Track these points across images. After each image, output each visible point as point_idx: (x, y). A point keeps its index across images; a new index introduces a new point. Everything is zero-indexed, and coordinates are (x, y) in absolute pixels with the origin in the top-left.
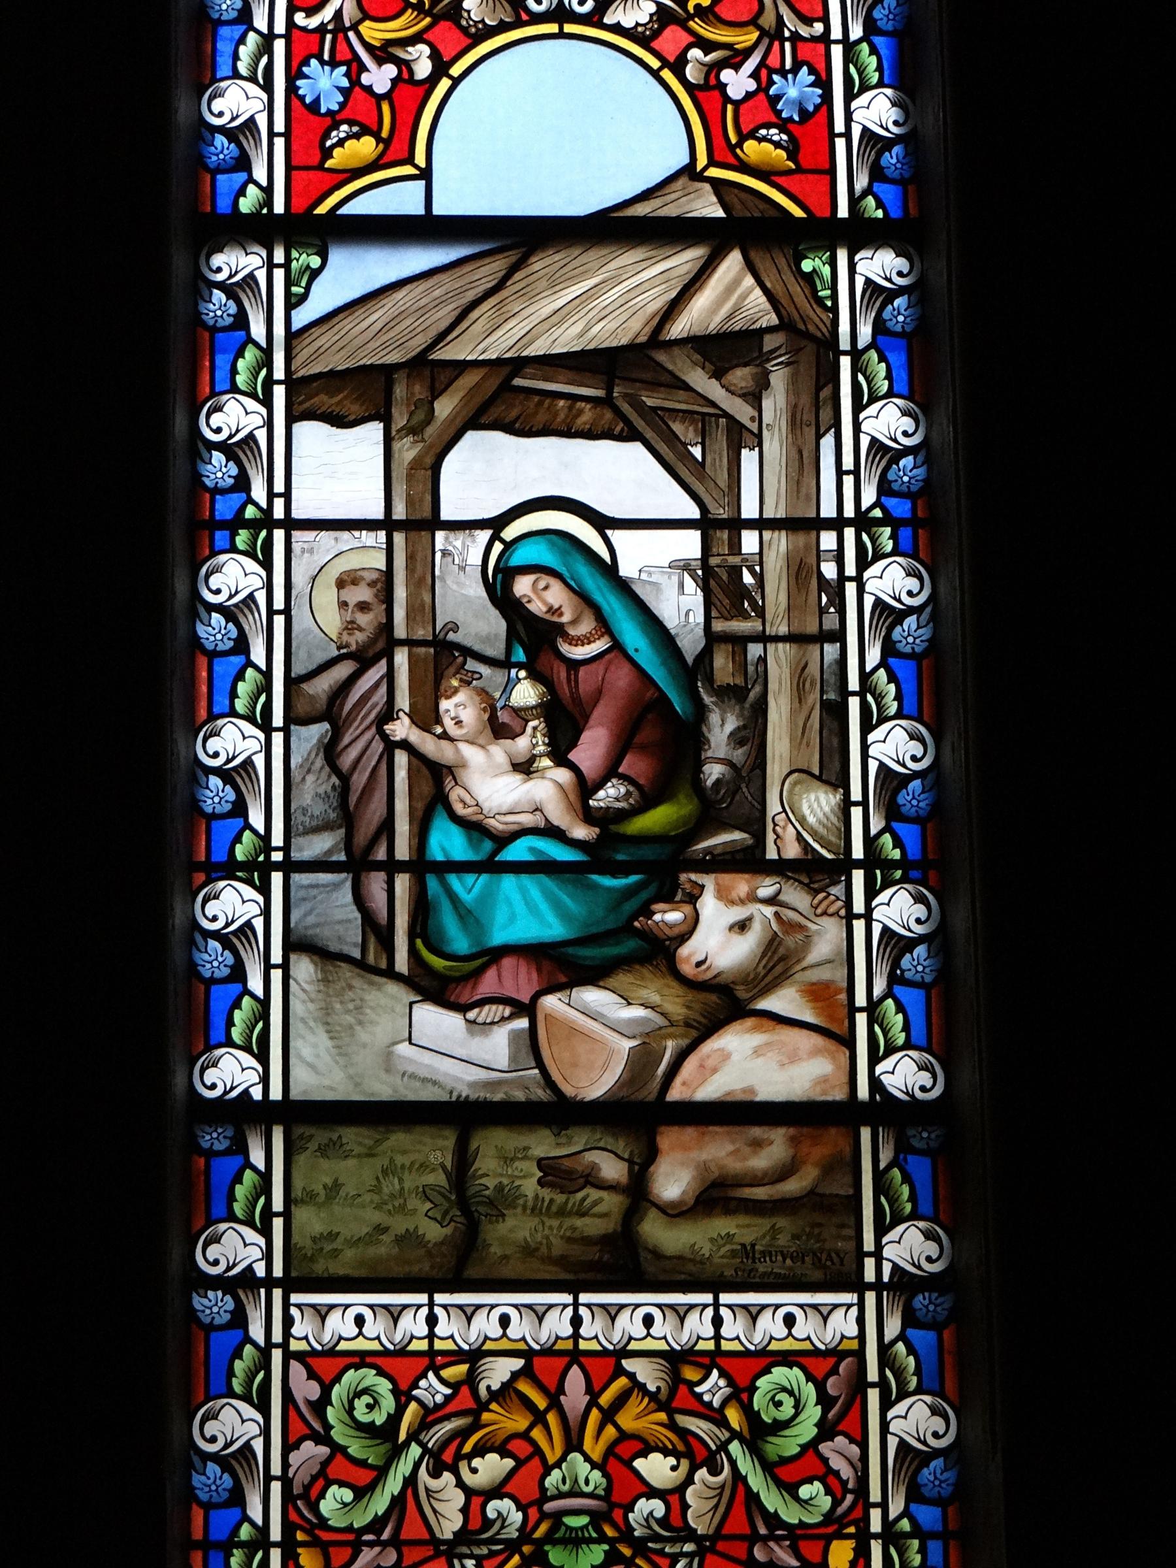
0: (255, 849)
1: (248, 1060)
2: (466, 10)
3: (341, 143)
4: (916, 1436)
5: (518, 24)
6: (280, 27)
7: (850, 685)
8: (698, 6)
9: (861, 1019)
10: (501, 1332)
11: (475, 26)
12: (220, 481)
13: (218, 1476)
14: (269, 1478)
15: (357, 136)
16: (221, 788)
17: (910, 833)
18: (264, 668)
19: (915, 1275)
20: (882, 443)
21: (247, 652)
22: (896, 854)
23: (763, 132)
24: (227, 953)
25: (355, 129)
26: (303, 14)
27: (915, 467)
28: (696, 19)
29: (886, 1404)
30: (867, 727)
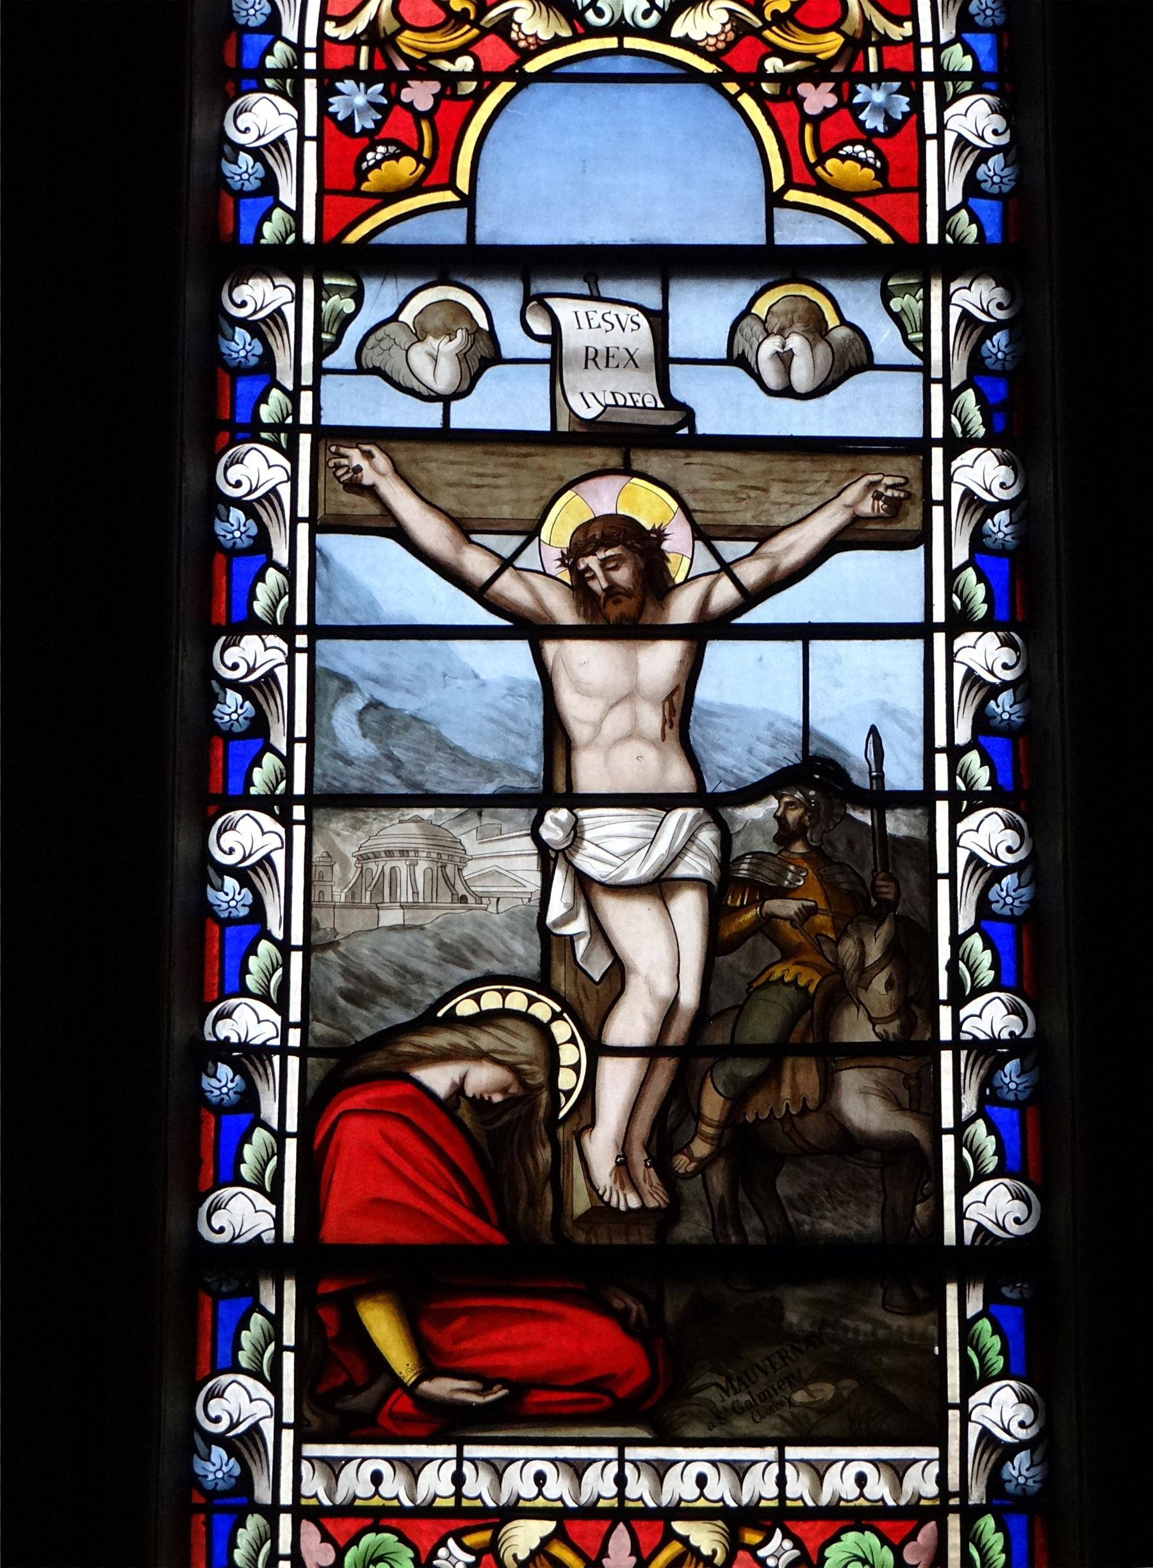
0: (264, 1336)
1: (259, 1390)
2: (516, 23)
3: (378, 164)
4: (995, 1221)
5: (575, 38)
6: (311, 41)
7: (926, 127)
8: (775, 13)
9: (948, 1142)
10: (535, 1490)
11: (526, 39)
12: (238, 541)
13: (237, 892)
14: (295, 520)
15: (396, 157)
16: (230, 1077)
17: (984, 44)
18: (293, 207)
19: (998, 1238)
20: (979, 678)
21: (269, 551)
22: (967, 64)
23: (848, 149)
24: (245, 890)
25: (392, 149)
26: (333, 24)
27: (1019, 887)
28: (774, 28)
29: (956, 817)
30: (964, 1185)
